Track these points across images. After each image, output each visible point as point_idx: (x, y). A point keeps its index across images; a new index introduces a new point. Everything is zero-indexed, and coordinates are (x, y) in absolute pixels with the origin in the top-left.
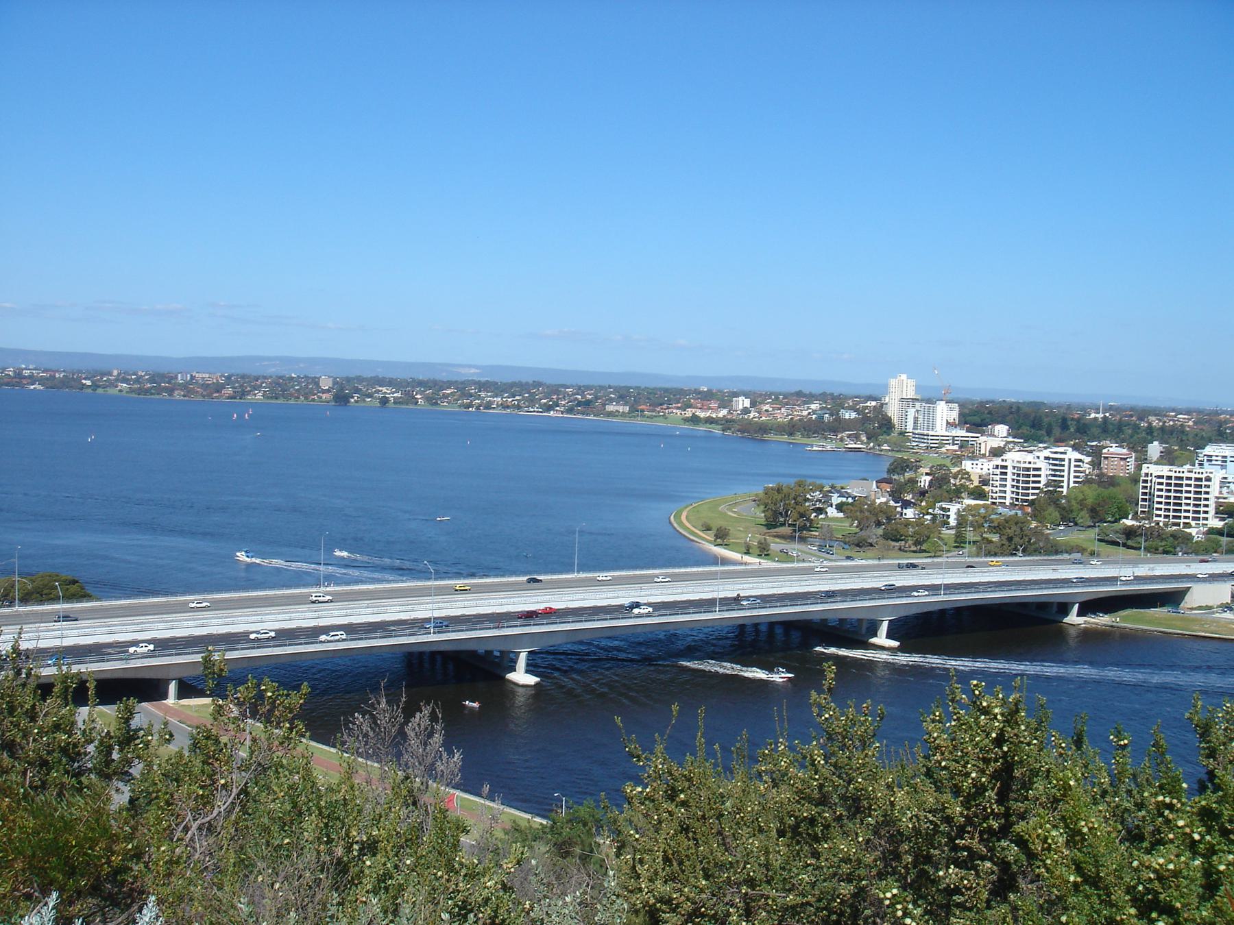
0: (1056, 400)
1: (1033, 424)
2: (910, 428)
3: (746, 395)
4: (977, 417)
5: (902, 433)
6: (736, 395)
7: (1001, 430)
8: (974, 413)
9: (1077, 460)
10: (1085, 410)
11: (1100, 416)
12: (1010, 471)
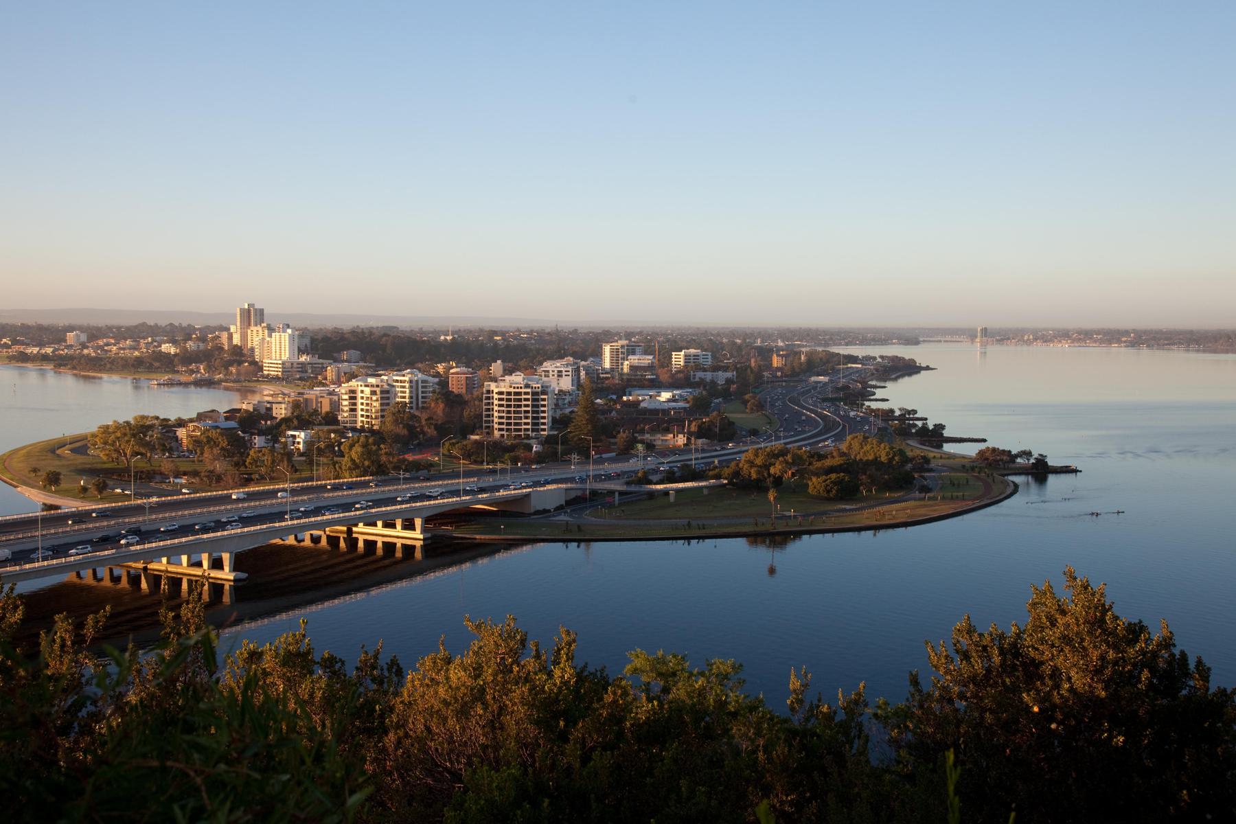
1: (380, 348)
9: (423, 382)
10: (438, 333)
11: (449, 338)
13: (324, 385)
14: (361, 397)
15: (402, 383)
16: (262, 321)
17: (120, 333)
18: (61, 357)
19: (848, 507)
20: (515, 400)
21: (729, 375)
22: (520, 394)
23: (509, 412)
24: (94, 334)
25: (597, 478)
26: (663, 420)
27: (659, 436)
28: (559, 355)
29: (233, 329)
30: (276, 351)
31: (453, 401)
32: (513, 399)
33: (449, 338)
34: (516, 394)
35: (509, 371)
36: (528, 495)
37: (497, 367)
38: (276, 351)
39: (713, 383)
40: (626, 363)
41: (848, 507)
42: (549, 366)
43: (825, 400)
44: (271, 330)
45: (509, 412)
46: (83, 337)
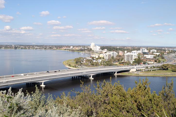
0: (113, 46)
1: (110, 49)
2: (94, 50)
3: (72, 46)
4: (103, 48)
5: (93, 51)
6: (71, 46)
7: (106, 50)
8: (102, 48)
10: (117, 47)
12: (107, 56)
14: (106, 55)
21: (159, 53)
26: (150, 60)
28: (134, 50)
29: (91, 46)
31: (120, 56)
32: (128, 56)
35: (127, 52)
37: (126, 52)
39: (157, 55)
42: (133, 51)
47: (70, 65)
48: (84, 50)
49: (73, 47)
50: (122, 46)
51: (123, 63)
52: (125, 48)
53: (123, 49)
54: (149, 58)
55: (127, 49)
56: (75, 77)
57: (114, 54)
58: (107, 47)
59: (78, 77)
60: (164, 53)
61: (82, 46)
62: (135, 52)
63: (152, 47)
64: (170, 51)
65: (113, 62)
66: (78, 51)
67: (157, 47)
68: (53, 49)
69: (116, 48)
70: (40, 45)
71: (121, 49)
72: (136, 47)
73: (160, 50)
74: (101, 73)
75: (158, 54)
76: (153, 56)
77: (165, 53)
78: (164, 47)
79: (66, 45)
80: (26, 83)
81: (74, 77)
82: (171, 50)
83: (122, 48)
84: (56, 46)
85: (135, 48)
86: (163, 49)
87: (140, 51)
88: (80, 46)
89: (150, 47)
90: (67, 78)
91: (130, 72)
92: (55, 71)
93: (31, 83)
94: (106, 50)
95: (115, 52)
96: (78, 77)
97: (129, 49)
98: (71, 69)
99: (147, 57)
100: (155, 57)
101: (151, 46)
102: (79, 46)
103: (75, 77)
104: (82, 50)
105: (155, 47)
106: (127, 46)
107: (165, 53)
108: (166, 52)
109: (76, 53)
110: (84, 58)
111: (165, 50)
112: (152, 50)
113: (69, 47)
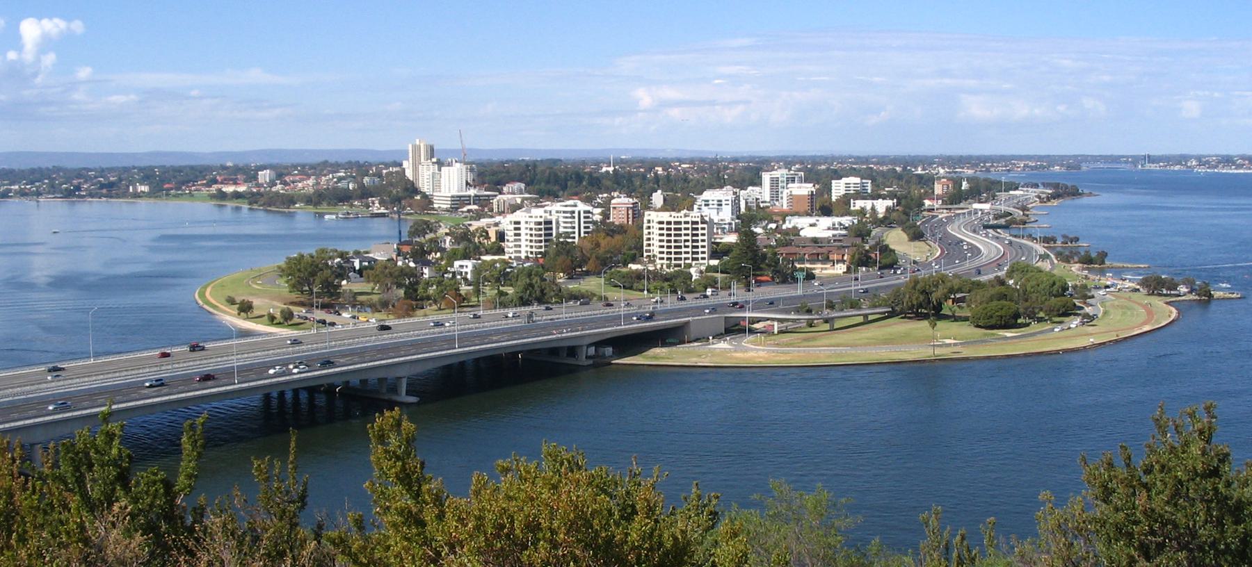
0: (573, 156)
1: (549, 179)
4: (491, 175)
6: (263, 168)
10: (598, 164)
13: (492, 217)
14: (522, 227)
15: (559, 212)
16: (432, 156)
17: (308, 170)
18: (253, 194)
19: (1009, 335)
20: (676, 253)
21: (889, 203)
22: (680, 223)
23: (669, 247)
24: (281, 173)
25: (788, 353)
26: (821, 250)
27: (819, 266)
28: (719, 183)
29: (405, 164)
30: (448, 184)
33: (611, 169)
34: (676, 223)
36: (687, 323)
38: (448, 184)
40: (786, 191)
41: (1009, 335)
42: (708, 195)
43: (986, 227)
44: (440, 164)
45: (669, 241)
46: (274, 175)
47: (245, 308)
48: (364, 194)
49: (280, 176)
50: (641, 155)
51: (639, 276)
52: (660, 170)
53: (637, 178)
54: (815, 240)
55: (668, 176)
56: (282, 394)
57: (568, 215)
58: (527, 166)
59: (304, 396)
60: (921, 198)
61: (349, 166)
62: (723, 198)
63: (842, 160)
64: (965, 185)
65: (561, 278)
66: (317, 204)
67: (882, 160)
68: (125, 194)
69: (590, 174)
70: (33, 171)
71: (630, 176)
72: (736, 160)
73: (899, 177)
74: (477, 360)
75: (882, 206)
76: (846, 221)
77: (927, 203)
78: (927, 161)
79: (229, 164)
80: (256, 401)
81: (289, 396)
82: (969, 180)
83: (637, 174)
84: (147, 175)
85: (726, 168)
86: (919, 171)
87: (757, 189)
88: (336, 167)
89: (833, 159)
90: (234, 402)
91: (1136, 271)
92: (163, 350)
93: (304, 388)
94: (512, 193)
95: (579, 203)
96: (304, 396)
97: (686, 180)
98: (260, 335)
99: (808, 233)
100: (860, 232)
101: (837, 154)
102: (325, 164)
103: (282, 394)
104: (342, 197)
105: (866, 160)
106: (674, 155)
107: (927, 203)
108: (938, 189)
109: (303, 216)
110: (357, 254)
111: (927, 181)
112: (845, 180)
113: (250, 174)
